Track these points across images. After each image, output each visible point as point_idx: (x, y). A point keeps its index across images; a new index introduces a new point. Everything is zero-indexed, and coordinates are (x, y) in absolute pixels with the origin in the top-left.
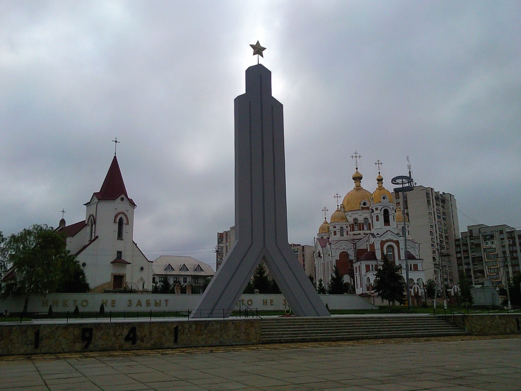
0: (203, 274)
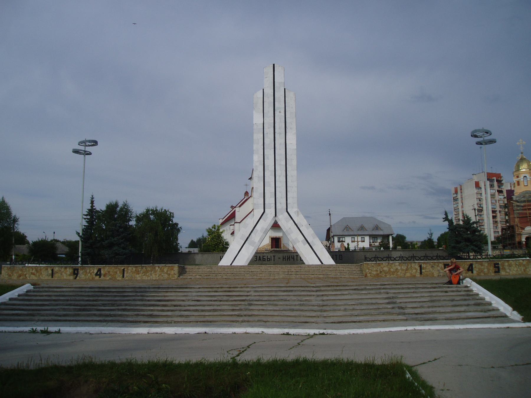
0: (381, 233)
